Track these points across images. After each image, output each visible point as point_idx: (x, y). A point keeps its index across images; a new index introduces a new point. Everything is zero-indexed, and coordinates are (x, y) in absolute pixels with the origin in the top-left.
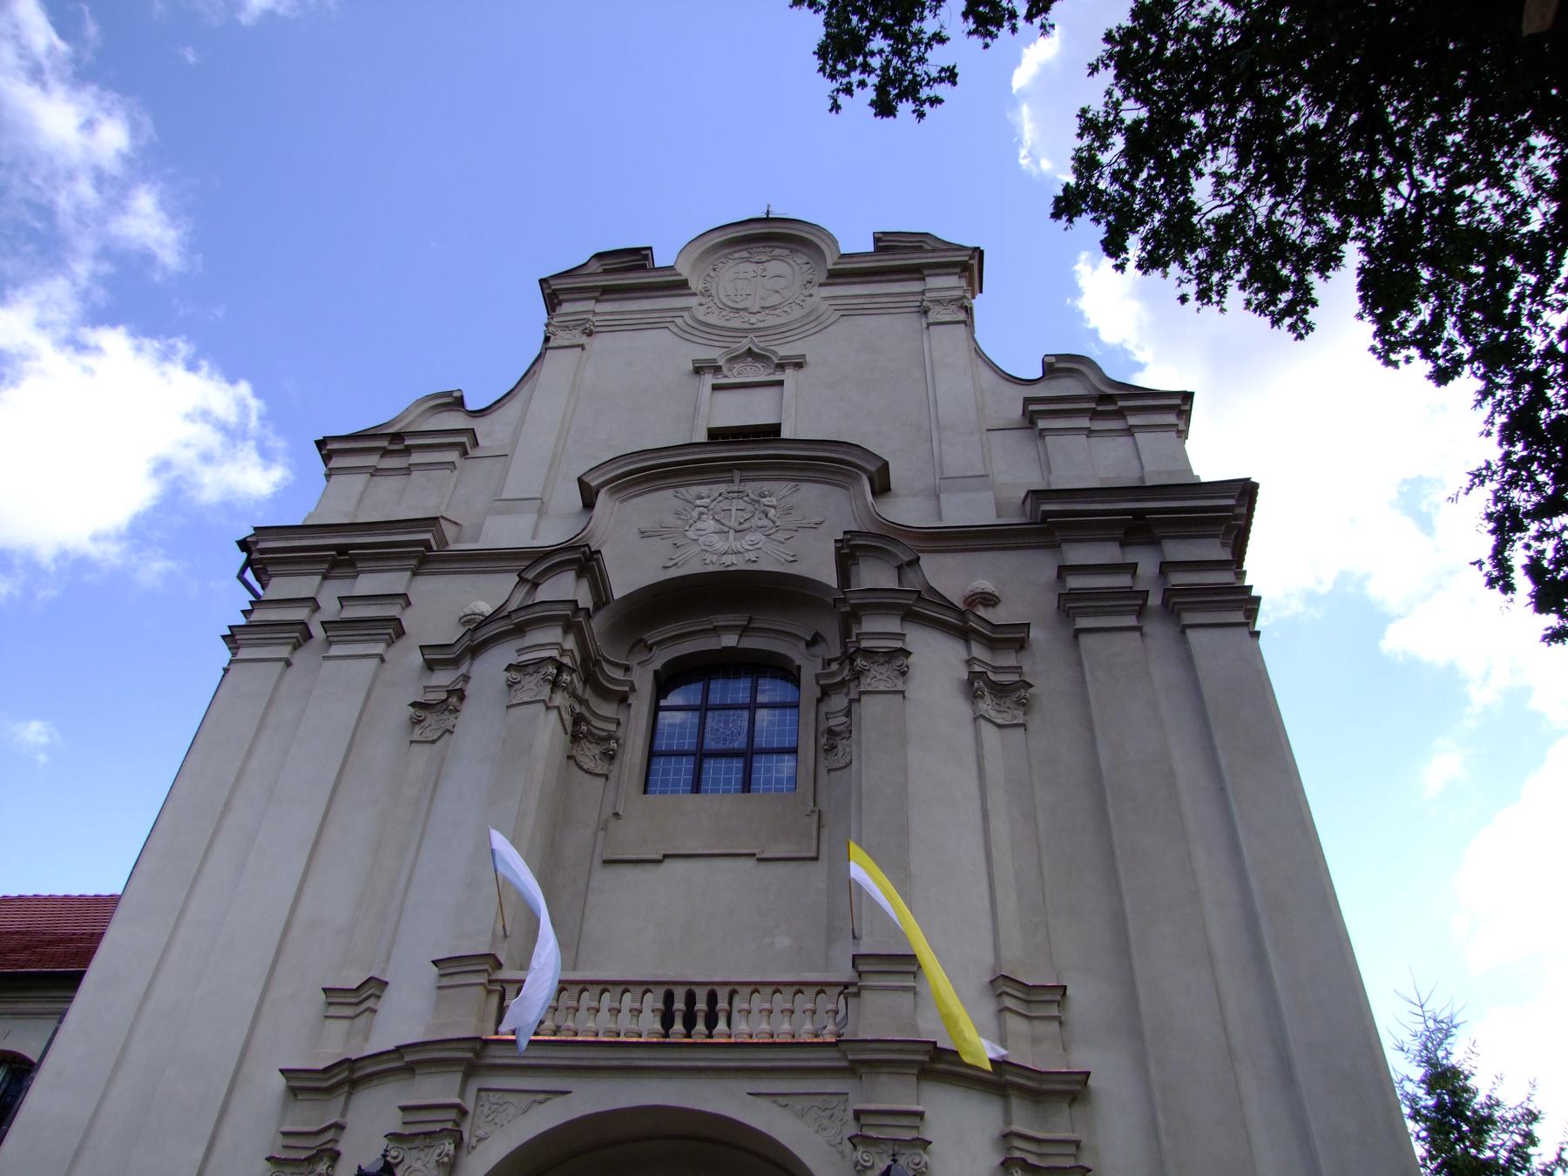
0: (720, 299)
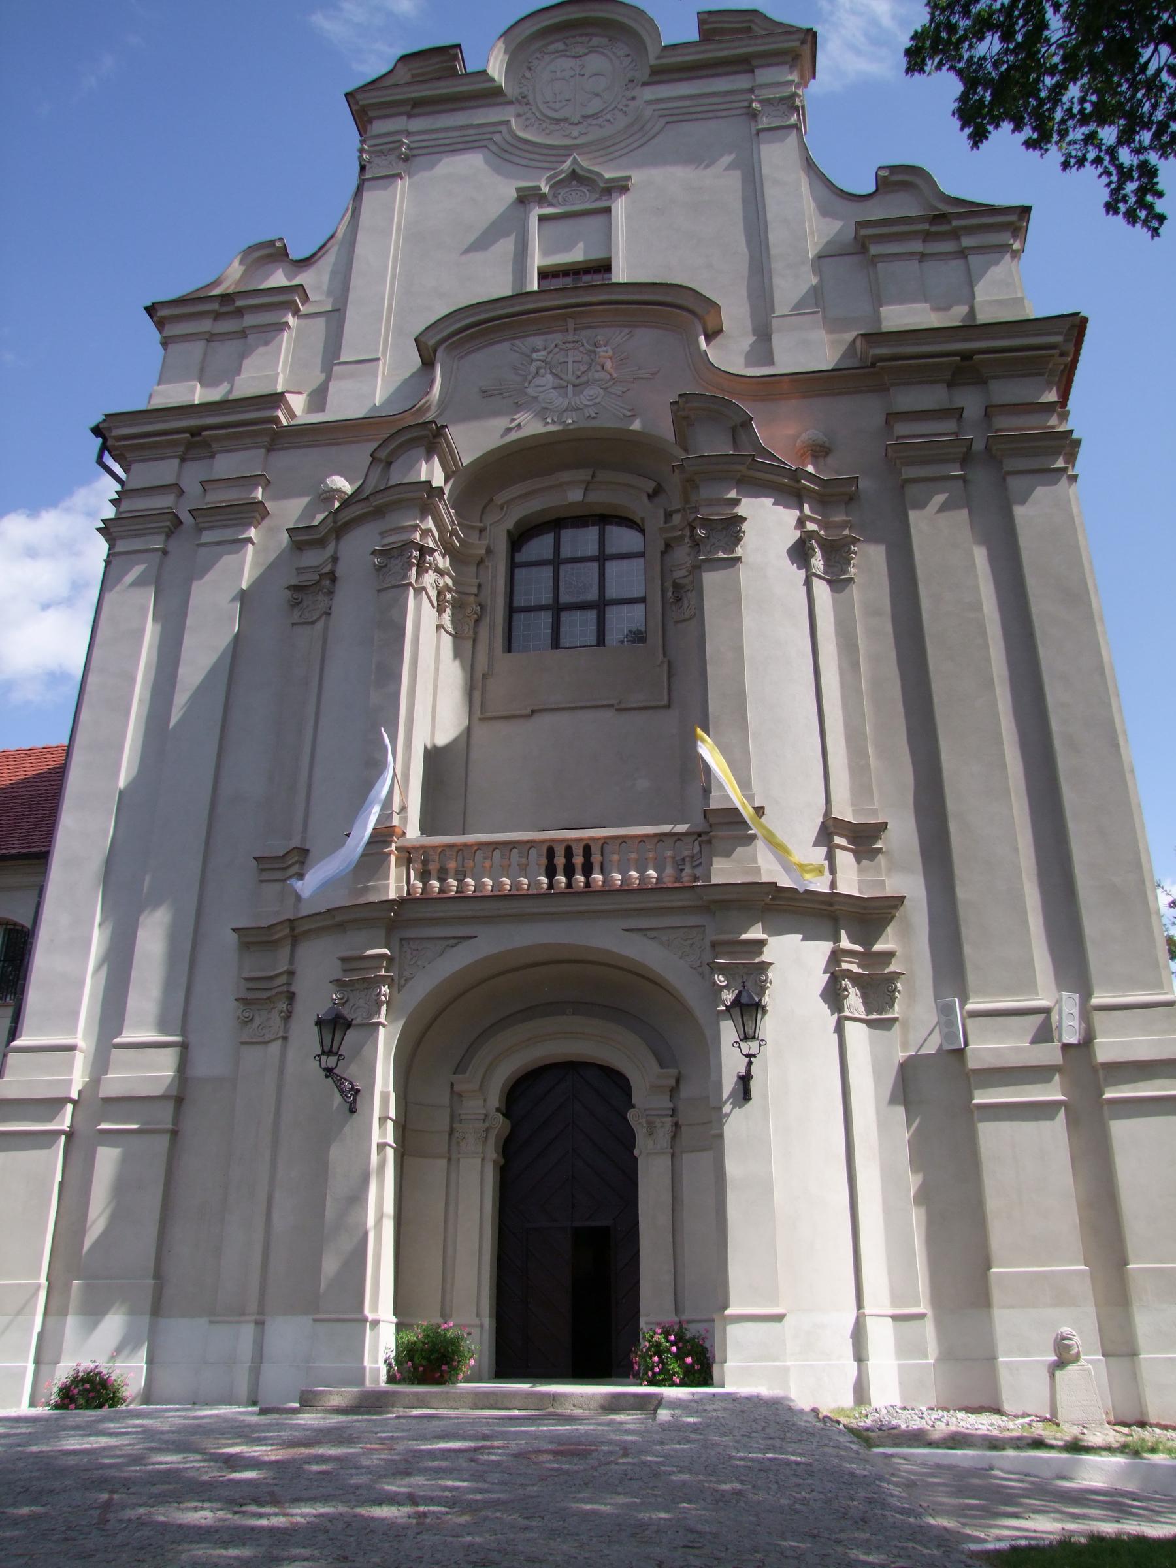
0: (538, 107)
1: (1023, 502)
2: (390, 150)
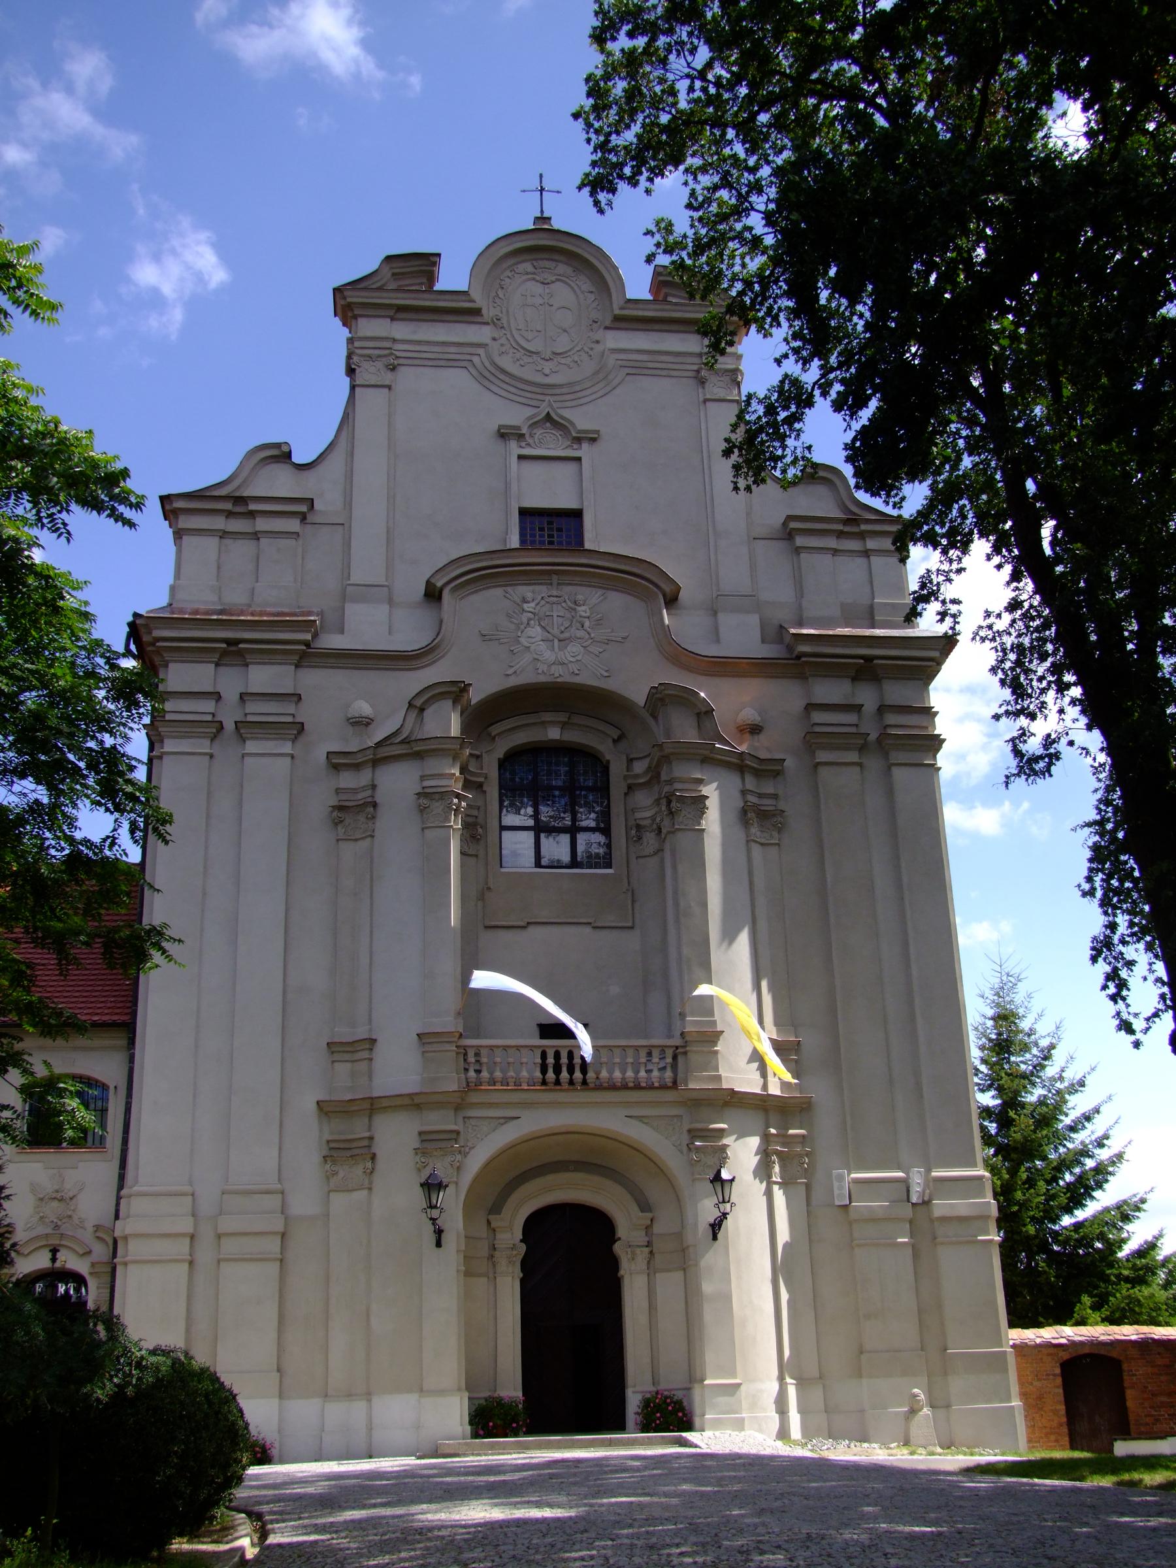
2: (380, 356)
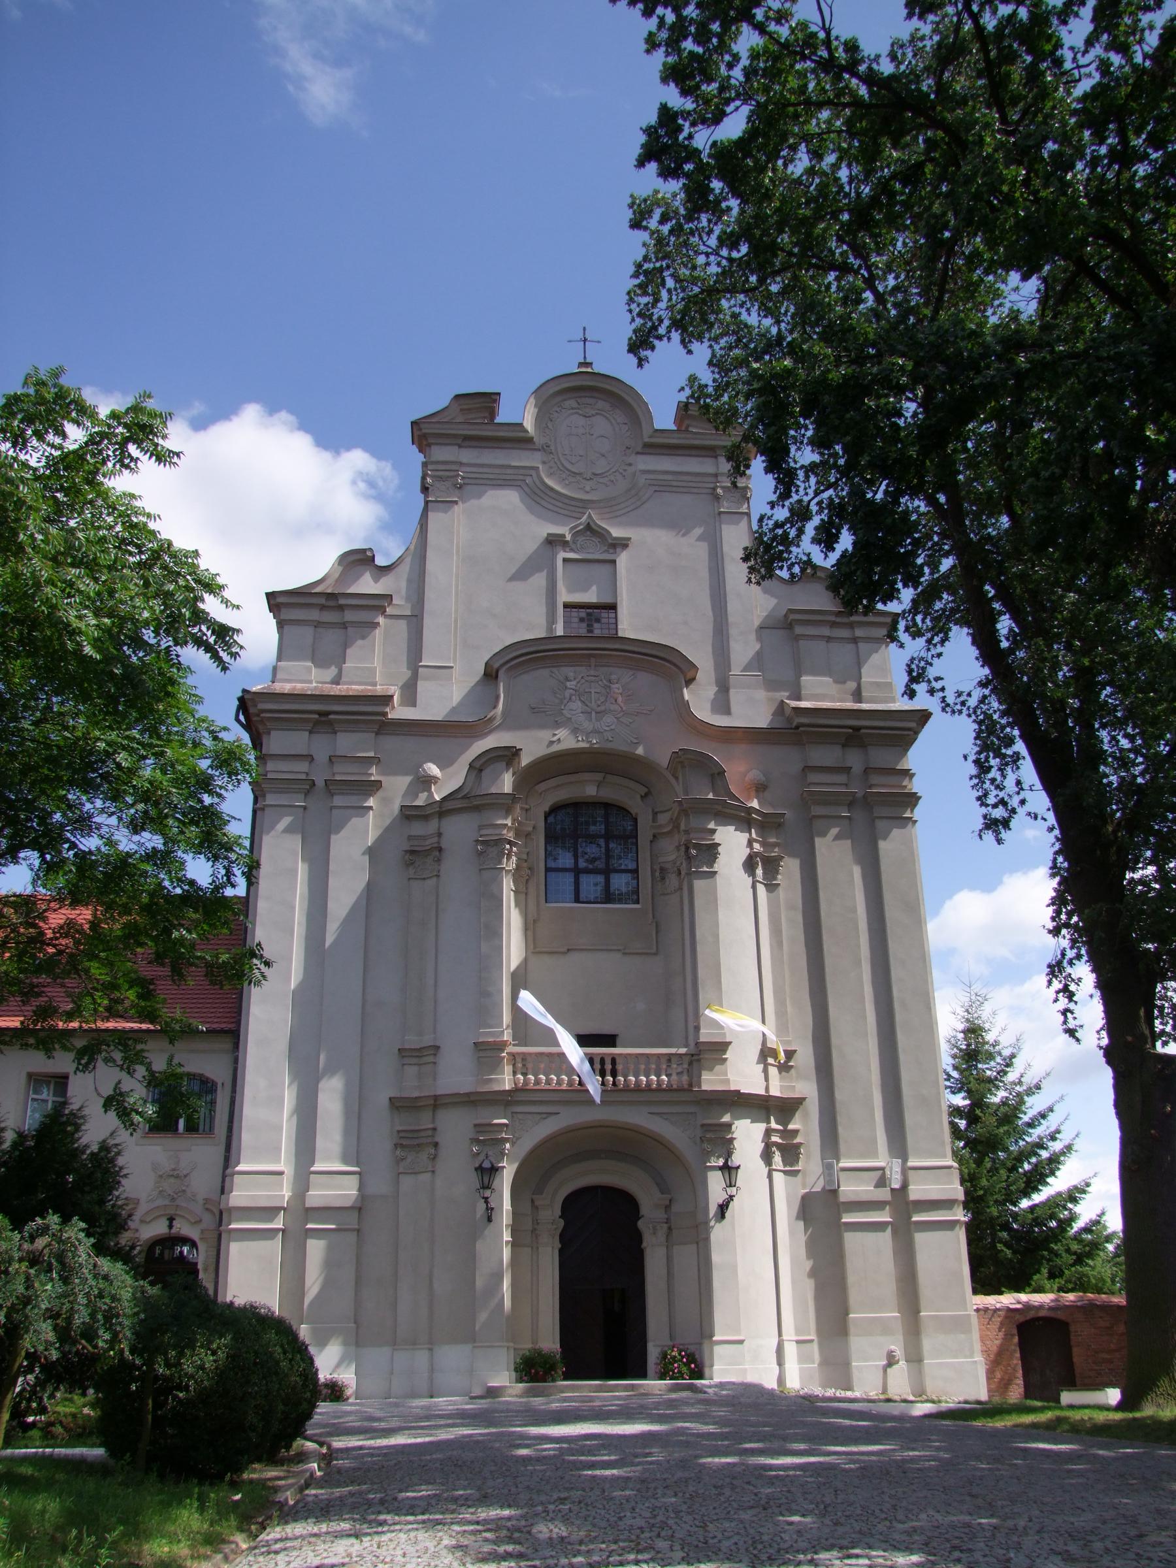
1: (885, 838)
